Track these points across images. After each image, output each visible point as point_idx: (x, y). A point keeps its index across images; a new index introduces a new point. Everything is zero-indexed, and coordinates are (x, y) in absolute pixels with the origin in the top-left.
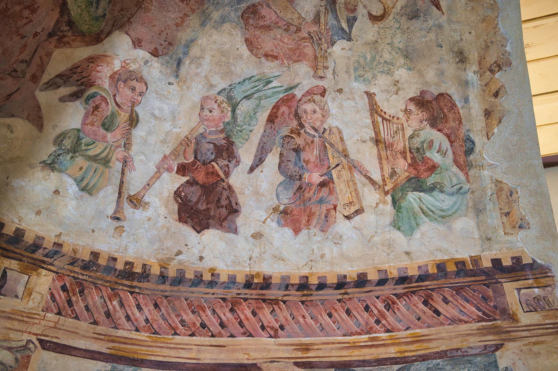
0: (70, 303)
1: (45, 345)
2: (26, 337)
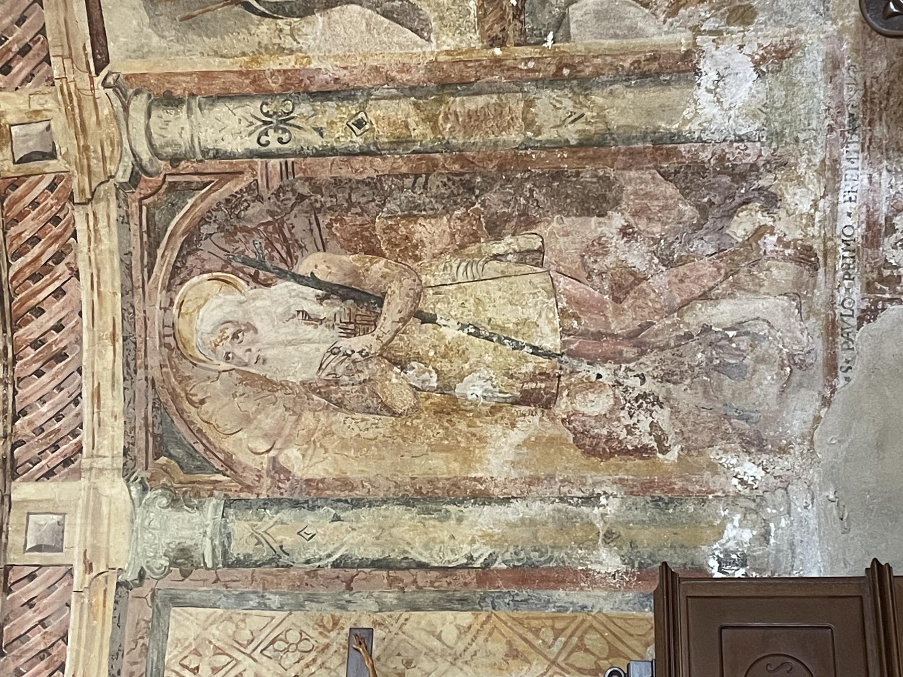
0: (24, 51)
1: (101, 61)
2: (100, 92)
